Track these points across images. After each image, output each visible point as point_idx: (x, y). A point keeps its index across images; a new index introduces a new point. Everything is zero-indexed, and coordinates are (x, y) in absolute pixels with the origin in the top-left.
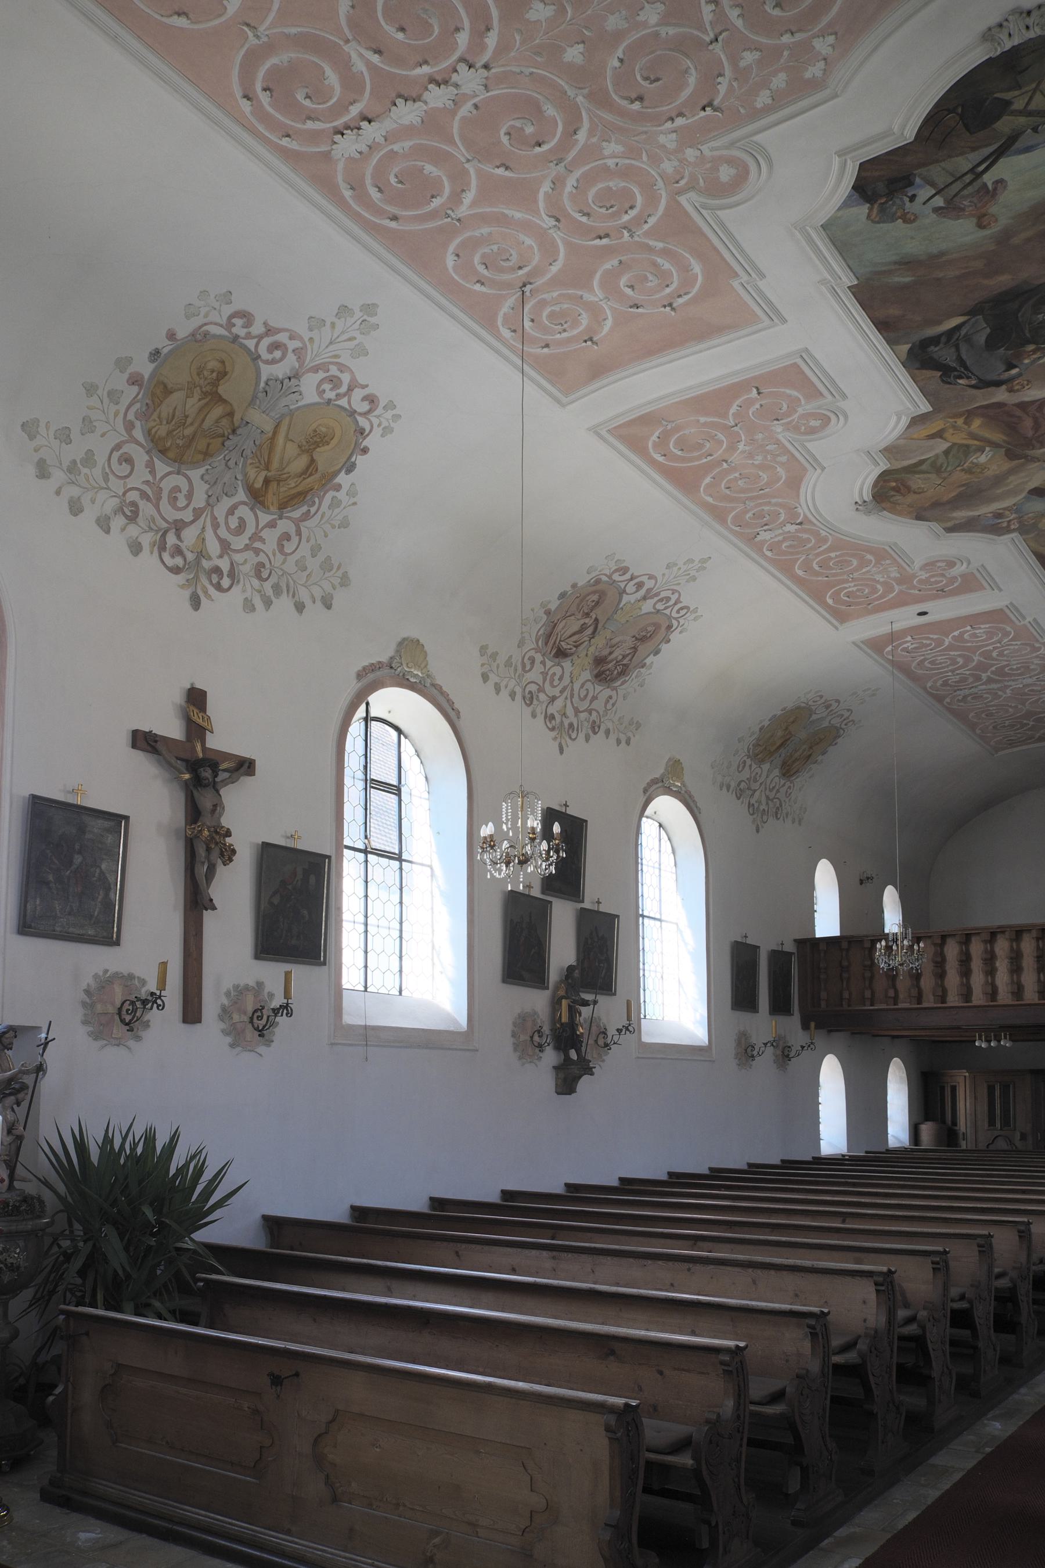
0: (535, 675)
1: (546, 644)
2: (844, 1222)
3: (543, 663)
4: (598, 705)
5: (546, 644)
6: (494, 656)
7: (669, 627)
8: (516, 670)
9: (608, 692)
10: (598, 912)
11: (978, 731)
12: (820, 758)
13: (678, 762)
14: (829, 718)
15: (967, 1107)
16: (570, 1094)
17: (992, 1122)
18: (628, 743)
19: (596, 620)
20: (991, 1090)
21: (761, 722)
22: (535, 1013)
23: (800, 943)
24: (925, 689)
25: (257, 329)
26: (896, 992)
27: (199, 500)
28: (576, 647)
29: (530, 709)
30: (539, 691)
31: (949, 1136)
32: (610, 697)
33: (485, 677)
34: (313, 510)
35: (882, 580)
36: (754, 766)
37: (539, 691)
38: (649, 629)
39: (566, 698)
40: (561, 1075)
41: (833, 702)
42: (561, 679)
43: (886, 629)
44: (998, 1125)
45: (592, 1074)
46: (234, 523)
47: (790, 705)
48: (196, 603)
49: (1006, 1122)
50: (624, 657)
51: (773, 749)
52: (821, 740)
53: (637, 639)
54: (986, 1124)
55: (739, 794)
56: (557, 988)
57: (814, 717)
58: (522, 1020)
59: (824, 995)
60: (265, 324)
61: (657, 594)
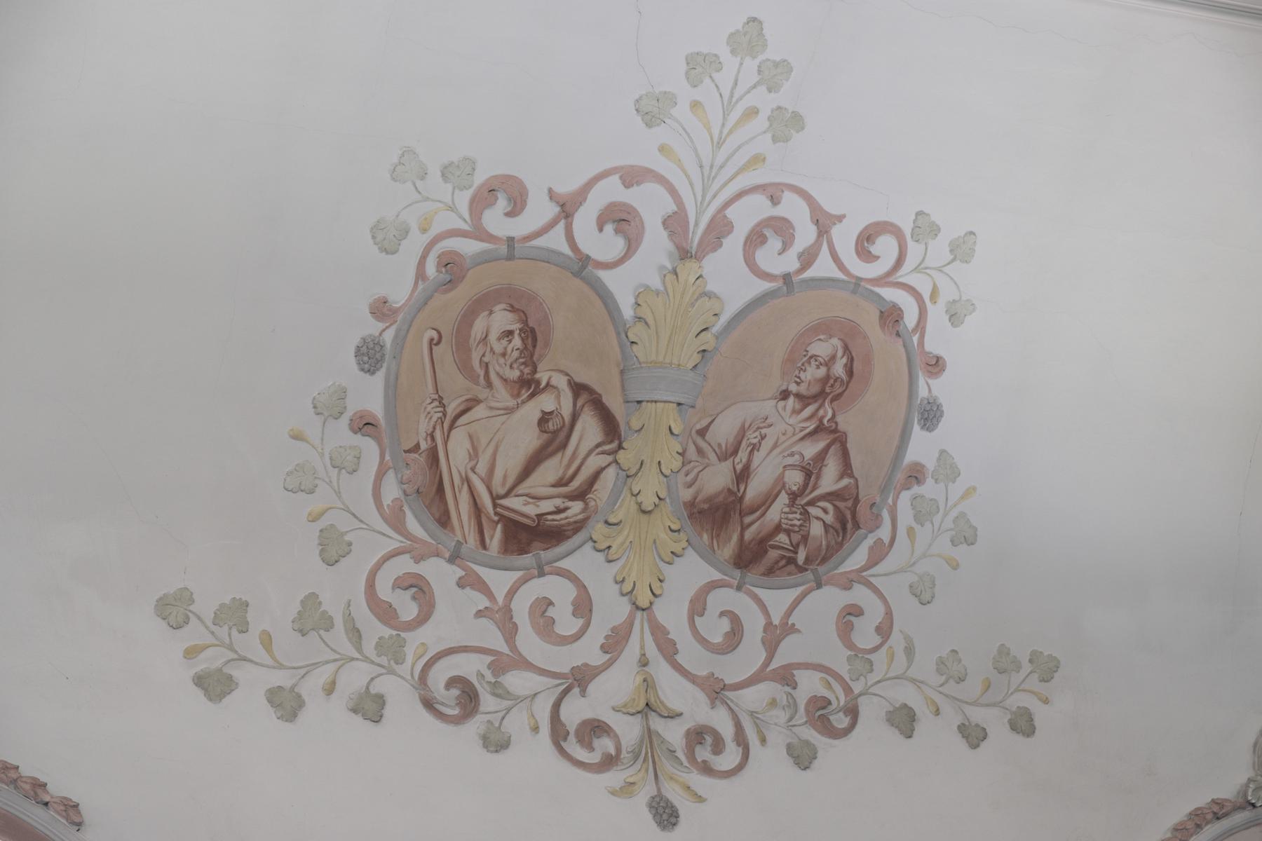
0: (456, 619)
1: (444, 521)
3: (470, 582)
5: (444, 521)
6: (235, 614)
7: (891, 316)
8: (355, 634)
9: (828, 601)
18: (1023, 724)
19: (578, 389)
25: (539, 211)
27: (611, 609)
28: (581, 495)
29: (475, 726)
30: (500, 665)
33: (215, 686)
34: (884, 533)
37: (500, 665)
38: (822, 349)
39: (644, 662)
42: (583, 607)
46: (716, 629)
48: (666, 815)
50: (811, 472)
53: (804, 400)
60: (551, 194)
61: (719, 229)
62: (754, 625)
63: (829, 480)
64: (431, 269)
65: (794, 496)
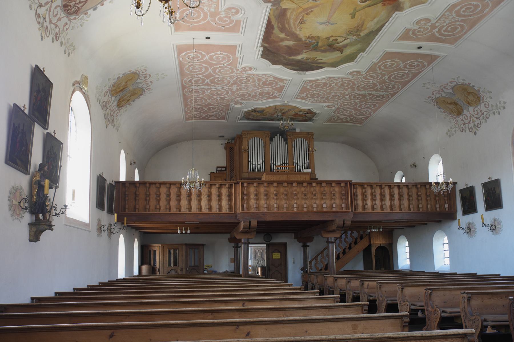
2: (243, 305)
4: (61, 24)
10: (54, 137)
11: (186, 109)
12: (132, 103)
13: (86, 77)
14: (144, 83)
15: (159, 259)
16: (36, 242)
17: (170, 264)
20: (170, 253)
21: (120, 74)
22: (22, 188)
23: (116, 182)
24: (182, 81)
26: (160, 206)
31: (153, 270)
32: (66, 24)
35: (206, 11)
36: (110, 96)
40: (34, 229)
41: (148, 75)
43: (190, 42)
44: (172, 265)
45: (52, 230)
47: (133, 70)
49: (175, 264)
51: (118, 90)
52: (135, 94)
54: (168, 265)
55: (103, 107)
56: (33, 176)
57: (139, 81)
58: (15, 191)
59: (127, 206)
62: (479, 111)
63: (79, 6)
64: (331, 39)
65: (76, 4)
